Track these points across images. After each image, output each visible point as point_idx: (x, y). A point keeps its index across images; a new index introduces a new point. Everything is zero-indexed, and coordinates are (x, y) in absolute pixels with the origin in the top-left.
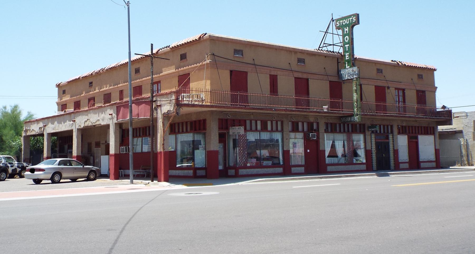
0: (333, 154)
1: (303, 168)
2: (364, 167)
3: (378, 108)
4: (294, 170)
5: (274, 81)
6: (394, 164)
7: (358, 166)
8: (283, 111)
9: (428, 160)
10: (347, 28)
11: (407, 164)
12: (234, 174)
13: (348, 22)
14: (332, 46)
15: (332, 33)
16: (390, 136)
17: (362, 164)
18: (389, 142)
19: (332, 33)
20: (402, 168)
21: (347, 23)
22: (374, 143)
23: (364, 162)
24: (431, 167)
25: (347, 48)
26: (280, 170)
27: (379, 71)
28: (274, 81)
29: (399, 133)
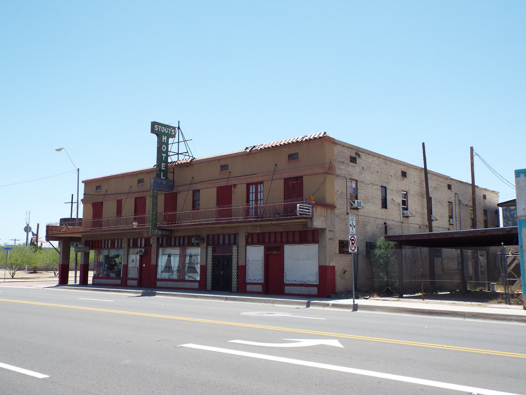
0: (168, 268)
1: (136, 281)
2: (196, 285)
3: (220, 214)
4: (130, 282)
5: (119, 203)
6: (237, 284)
7: (189, 283)
8: (143, 229)
9: (301, 283)
10: (166, 137)
11: (314, 288)
12: (316, 293)
13: (166, 131)
14: (179, 153)
15: (178, 143)
16: (235, 248)
17: (195, 281)
18: (232, 256)
19: (178, 143)
20: (288, 293)
21: (165, 131)
22: (211, 257)
23: (197, 280)
24: (307, 293)
25: (164, 158)
26: (119, 282)
27: (224, 168)
28: (119, 203)
29: (247, 244)
